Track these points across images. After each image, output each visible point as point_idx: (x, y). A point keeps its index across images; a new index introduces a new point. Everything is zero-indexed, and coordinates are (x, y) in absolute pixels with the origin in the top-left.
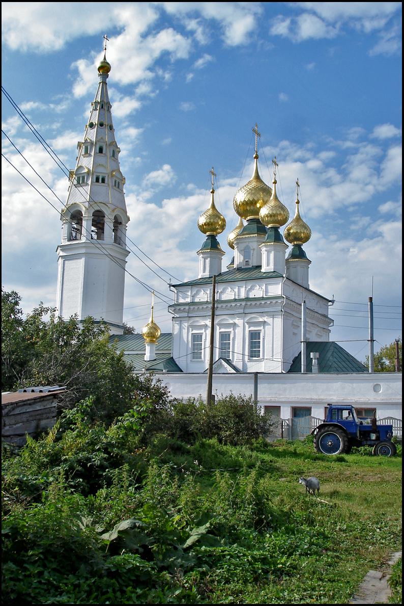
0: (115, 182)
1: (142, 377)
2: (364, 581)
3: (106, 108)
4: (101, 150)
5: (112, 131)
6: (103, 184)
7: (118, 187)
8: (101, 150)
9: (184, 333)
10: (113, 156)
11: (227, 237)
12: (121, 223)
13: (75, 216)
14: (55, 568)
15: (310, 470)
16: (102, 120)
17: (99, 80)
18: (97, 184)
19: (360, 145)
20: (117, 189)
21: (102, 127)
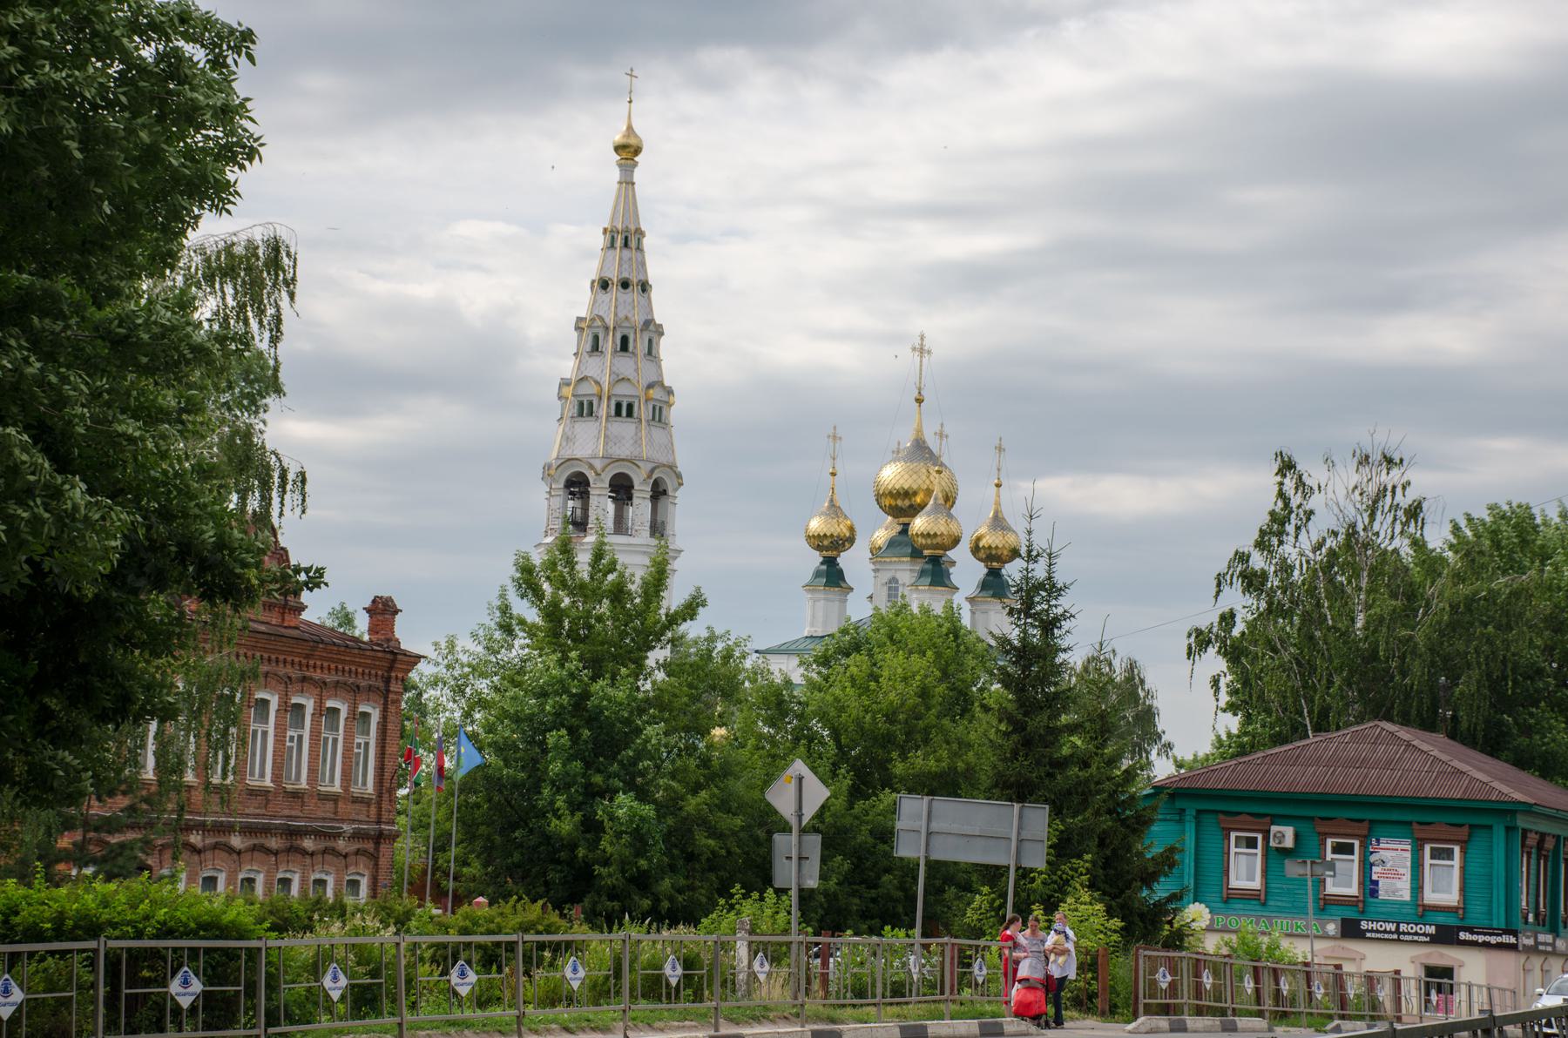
0: (654, 408)
1: (275, 894)
2: (228, 212)
3: (633, 244)
4: (624, 345)
5: (646, 295)
6: (629, 419)
7: (660, 421)
8: (624, 345)
9: (366, 890)
10: (650, 353)
11: (854, 562)
12: (665, 492)
13: (577, 486)
14: (914, 516)
15: (1266, 979)
16: (625, 275)
17: (615, 174)
18: (618, 419)
19: (252, 927)
20: (658, 424)
21: (627, 291)
